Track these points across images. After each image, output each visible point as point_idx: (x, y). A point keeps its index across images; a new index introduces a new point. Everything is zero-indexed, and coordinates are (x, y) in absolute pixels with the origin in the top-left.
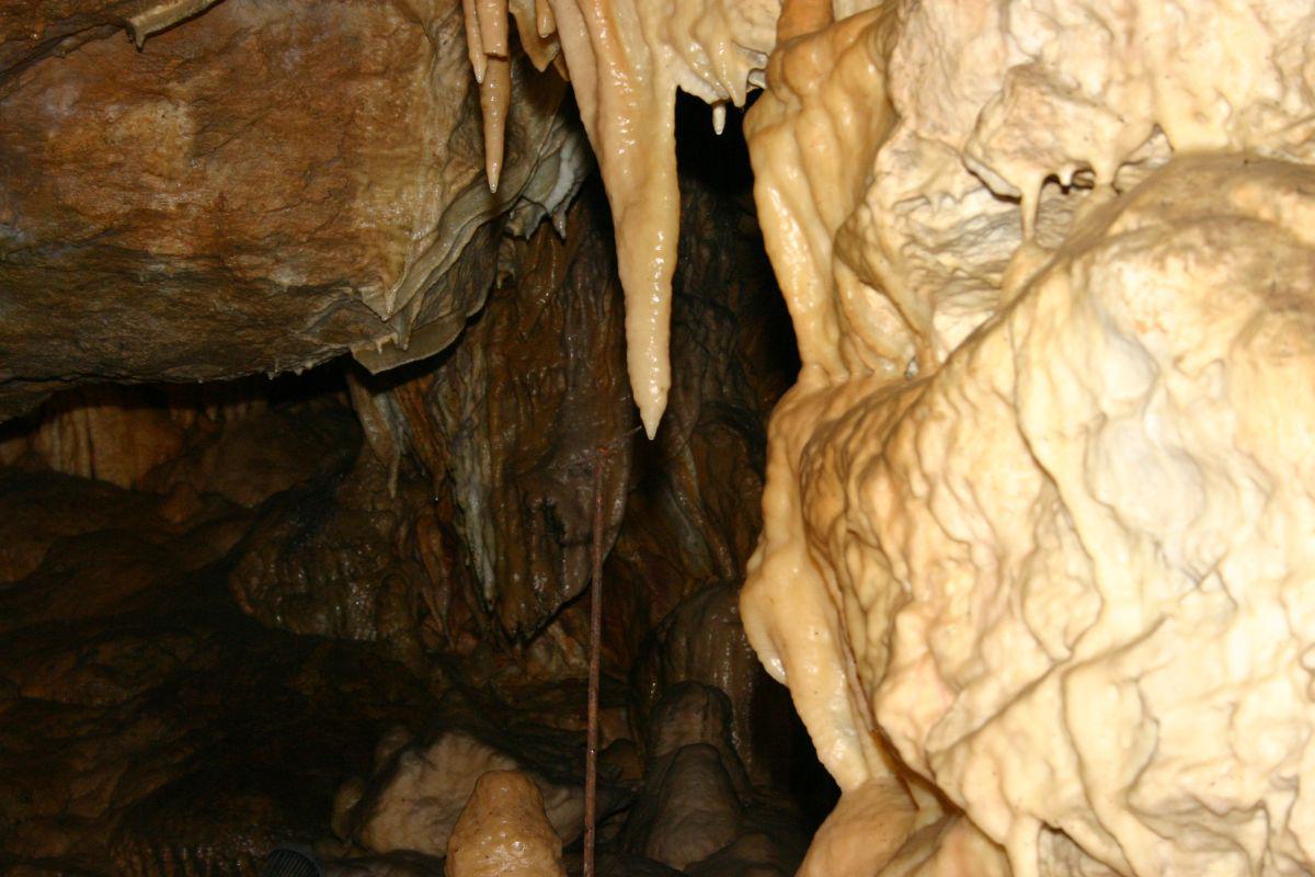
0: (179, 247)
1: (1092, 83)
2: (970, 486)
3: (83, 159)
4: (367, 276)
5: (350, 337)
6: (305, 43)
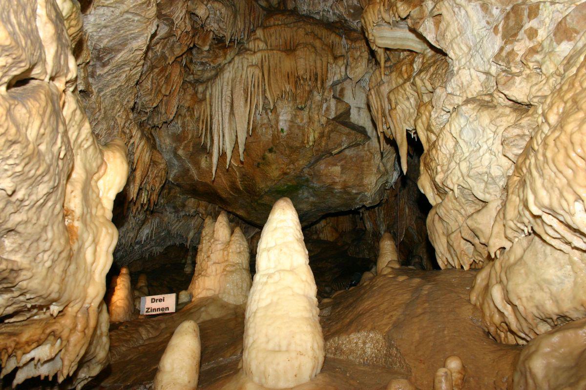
0: (339, 187)
1: (458, 93)
2: (446, 145)
3: (326, 175)
4: (366, 191)
5: (364, 202)
6: (356, 157)
